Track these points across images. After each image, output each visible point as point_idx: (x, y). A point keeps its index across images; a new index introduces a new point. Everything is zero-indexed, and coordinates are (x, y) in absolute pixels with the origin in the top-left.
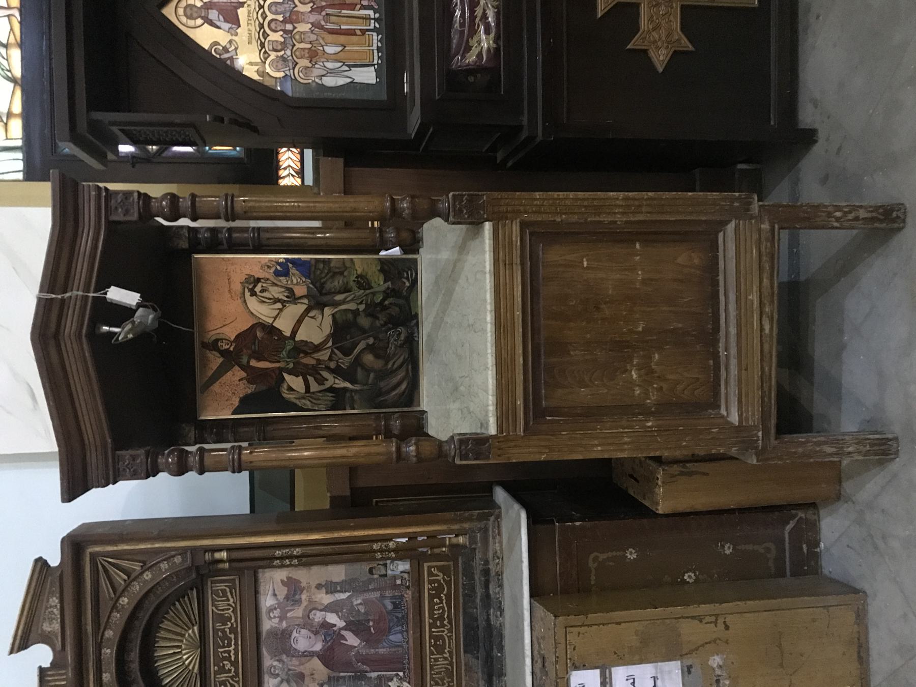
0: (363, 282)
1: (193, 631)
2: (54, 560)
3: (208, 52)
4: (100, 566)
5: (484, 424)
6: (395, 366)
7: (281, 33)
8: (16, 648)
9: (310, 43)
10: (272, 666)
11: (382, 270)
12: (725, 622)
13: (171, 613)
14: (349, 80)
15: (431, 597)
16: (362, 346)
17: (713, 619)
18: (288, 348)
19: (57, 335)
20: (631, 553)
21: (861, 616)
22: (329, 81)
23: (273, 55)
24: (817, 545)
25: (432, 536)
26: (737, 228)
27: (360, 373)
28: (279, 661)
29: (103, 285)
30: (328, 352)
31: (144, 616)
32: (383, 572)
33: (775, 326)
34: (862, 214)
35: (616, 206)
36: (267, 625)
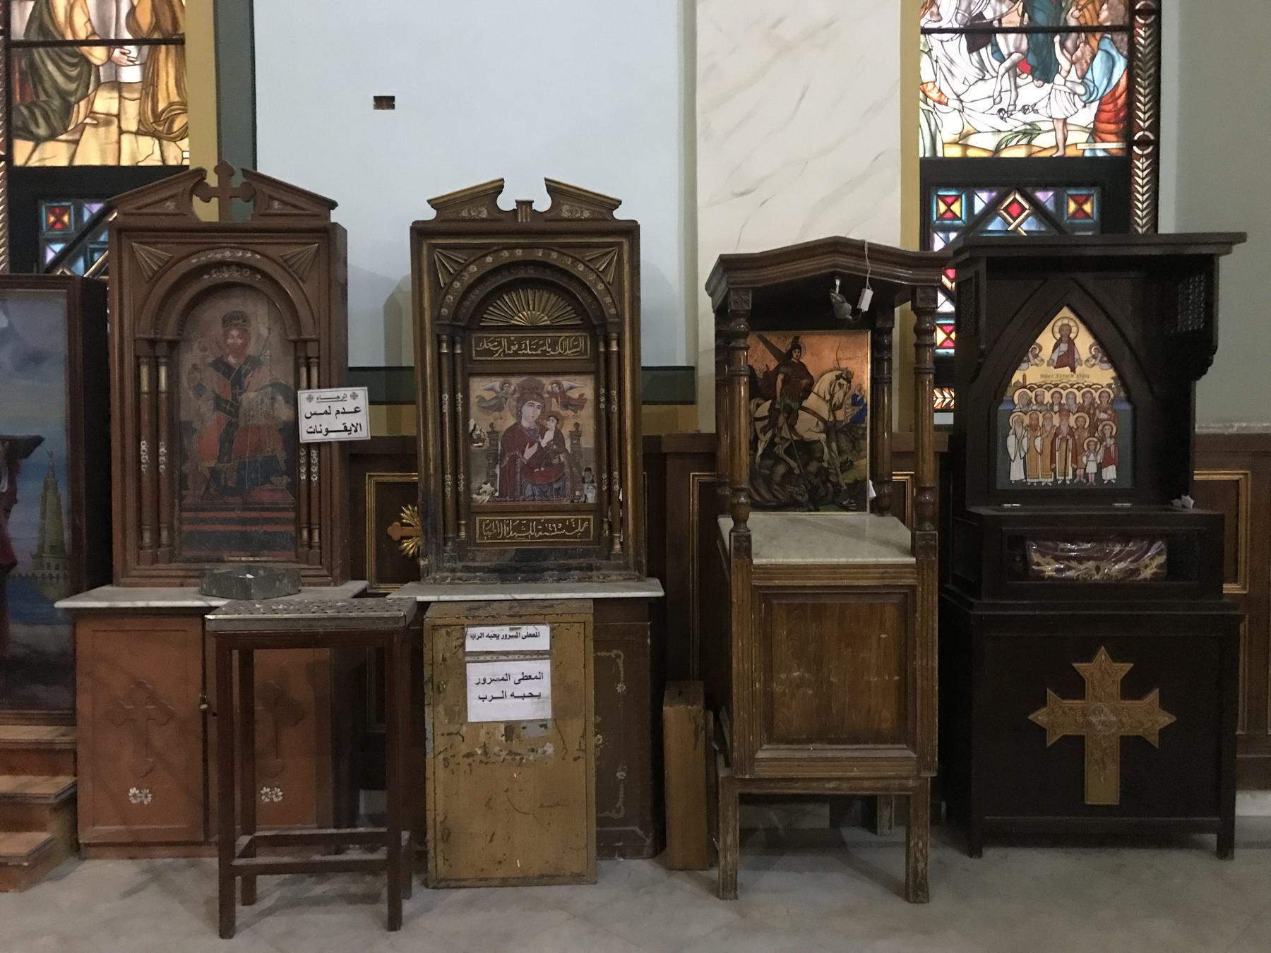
0: (847, 466)
1: (546, 320)
2: (619, 214)
3: (1033, 341)
4: (611, 249)
5: (757, 555)
6: (774, 491)
7: (1051, 402)
8: (548, 183)
9: (1043, 426)
10: (510, 384)
11: (857, 482)
12: (579, 757)
13: (562, 303)
14: (1013, 458)
15: (563, 521)
16: (793, 464)
17: (583, 747)
18: (793, 405)
19: (836, 252)
20: (621, 687)
21: (578, 879)
22: (1011, 441)
23: (1033, 395)
24: (624, 856)
25: (623, 521)
26: (910, 758)
27: (769, 462)
28: (515, 391)
29: (875, 285)
30: (788, 437)
31: (573, 288)
32: (587, 480)
33: (831, 792)
34: (921, 866)
35: (927, 661)
36: (547, 382)
